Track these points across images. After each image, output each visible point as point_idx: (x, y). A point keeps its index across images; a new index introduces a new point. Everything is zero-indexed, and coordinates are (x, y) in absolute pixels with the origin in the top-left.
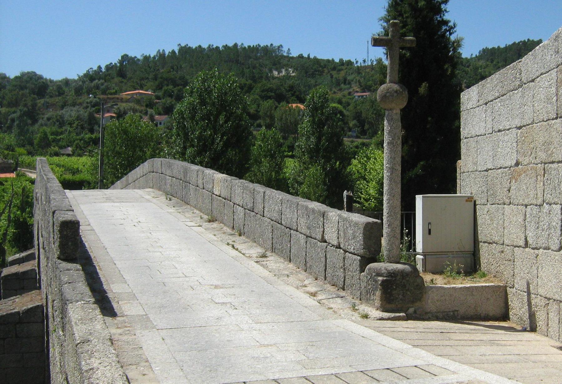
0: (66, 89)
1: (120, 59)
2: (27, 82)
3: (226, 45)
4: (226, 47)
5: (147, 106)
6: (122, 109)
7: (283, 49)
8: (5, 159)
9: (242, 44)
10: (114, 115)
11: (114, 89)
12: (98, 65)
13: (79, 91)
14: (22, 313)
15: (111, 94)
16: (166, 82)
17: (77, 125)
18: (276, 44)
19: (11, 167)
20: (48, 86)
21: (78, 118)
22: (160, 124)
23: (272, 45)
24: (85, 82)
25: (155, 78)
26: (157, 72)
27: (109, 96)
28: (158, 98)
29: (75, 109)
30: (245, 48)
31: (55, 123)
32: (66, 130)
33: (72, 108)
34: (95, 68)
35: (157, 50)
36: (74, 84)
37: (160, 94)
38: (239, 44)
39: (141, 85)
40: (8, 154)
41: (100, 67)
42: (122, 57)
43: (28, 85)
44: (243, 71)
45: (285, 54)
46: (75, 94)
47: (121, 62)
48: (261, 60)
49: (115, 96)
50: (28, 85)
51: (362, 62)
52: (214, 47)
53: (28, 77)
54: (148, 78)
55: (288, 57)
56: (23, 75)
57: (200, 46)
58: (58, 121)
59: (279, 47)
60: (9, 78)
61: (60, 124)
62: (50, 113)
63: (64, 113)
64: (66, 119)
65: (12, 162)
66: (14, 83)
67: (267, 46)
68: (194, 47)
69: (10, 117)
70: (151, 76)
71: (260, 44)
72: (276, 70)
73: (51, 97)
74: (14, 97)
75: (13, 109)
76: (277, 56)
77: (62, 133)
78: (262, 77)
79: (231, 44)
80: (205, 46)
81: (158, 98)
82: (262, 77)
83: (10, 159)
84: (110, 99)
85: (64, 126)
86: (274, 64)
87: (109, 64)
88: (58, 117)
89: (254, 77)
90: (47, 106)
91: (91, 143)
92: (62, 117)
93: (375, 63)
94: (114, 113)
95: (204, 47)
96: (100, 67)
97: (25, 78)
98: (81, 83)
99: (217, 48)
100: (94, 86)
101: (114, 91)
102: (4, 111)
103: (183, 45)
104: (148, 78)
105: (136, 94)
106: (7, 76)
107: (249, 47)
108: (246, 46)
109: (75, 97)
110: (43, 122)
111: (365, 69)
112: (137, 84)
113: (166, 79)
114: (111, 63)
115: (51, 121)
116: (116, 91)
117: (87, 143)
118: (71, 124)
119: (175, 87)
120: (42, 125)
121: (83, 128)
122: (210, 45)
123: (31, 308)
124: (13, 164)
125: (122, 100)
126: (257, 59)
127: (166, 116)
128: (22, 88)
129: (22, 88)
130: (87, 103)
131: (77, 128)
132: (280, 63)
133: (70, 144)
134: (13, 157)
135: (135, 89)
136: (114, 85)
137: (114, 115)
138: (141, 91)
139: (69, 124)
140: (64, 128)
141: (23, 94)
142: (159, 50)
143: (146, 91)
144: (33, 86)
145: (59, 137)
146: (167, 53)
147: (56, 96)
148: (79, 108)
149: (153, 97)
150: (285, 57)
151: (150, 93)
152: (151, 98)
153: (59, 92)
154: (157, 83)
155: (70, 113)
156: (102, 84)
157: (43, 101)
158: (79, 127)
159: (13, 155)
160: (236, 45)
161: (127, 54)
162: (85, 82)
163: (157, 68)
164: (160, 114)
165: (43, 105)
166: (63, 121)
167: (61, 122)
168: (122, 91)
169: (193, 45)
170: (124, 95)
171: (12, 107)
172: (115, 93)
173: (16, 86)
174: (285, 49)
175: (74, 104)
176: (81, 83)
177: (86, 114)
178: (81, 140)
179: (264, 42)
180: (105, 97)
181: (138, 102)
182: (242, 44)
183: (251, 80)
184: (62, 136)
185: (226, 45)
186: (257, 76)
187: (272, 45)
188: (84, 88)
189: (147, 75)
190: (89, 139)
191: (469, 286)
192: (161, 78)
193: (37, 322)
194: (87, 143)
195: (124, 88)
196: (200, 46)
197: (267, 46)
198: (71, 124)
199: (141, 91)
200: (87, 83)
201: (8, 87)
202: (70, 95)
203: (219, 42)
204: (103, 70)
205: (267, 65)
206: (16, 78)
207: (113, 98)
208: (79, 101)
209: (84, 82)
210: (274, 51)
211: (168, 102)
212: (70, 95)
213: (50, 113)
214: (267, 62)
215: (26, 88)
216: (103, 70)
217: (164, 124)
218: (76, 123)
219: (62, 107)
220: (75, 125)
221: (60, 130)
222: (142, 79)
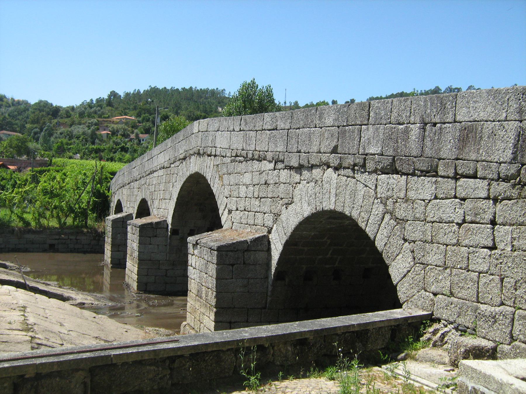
1: (109, 94)
2: (45, 107)
3: (184, 88)
4: (184, 89)
5: (133, 127)
6: (115, 128)
7: (225, 92)
8: (42, 157)
9: (196, 87)
10: (110, 133)
11: (107, 114)
14: (250, 242)
15: (105, 118)
16: (143, 112)
17: (83, 138)
18: (220, 88)
19: (46, 163)
20: (60, 110)
21: (84, 133)
22: (143, 140)
23: (217, 89)
24: (86, 109)
25: (135, 108)
26: (136, 105)
27: (104, 119)
28: (139, 122)
29: (81, 126)
30: (198, 90)
31: (66, 137)
32: (74, 142)
33: (79, 126)
34: (88, 101)
35: (134, 89)
36: (78, 110)
38: (194, 87)
39: (125, 113)
40: (44, 154)
41: (92, 100)
42: (111, 92)
44: (198, 106)
45: (227, 96)
47: (109, 96)
49: (108, 119)
50: (45, 109)
51: (283, 103)
52: (176, 88)
53: (45, 103)
54: (129, 109)
55: (229, 98)
56: (41, 101)
57: (165, 88)
58: (68, 135)
59: (222, 90)
60: (30, 104)
61: (70, 137)
62: (62, 129)
63: (73, 129)
64: (74, 133)
65: (47, 159)
67: (214, 89)
68: (161, 89)
69: (33, 131)
70: (132, 107)
72: (221, 107)
73: (62, 118)
74: (36, 117)
75: (35, 126)
77: (71, 144)
79: (187, 87)
80: (169, 88)
81: (139, 122)
82: (212, 111)
84: (105, 121)
85: (72, 139)
86: (219, 103)
87: (98, 98)
88: (68, 133)
89: (206, 111)
90: (59, 124)
91: (94, 152)
92: (71, 132)
93: (293, 104)
94: (110, 131)
96: (92, 100)
97: (42, 104)
98: (83, 109)
99: (177, 89)
100: (93, 112)
101: (108, 116)
102: (29, 127)
103: (153, 87)
104: (129, 109)
105: (123, 119)
106: (29, 102)
107: (201, 89)
108: (199, 88)
110: (57, 136)
111: (285, 109)
112: (122, 112)
113: (144, 110)
114: (100, 98)
115: (63, 135)
116: (109, 116)
117: (91, 152)
118: (78, 138)
119: (150, 115)
120: (56, 138)
121: (86, 141)
122: (172, 87)
123: (259, 238)
124: (48, 161)
125: (113, 123)
126: (206, 98)
128: (41, 111)
129: (41, 111)
130: (89, 123)
131: (82, 140)
132: (223, 102)
133: (78, 152)
134: (48, 156)
135: (122, 115)
136: (107, 111)
138: (127, 117)
139: (77, 137)
140: (73, 141)
141: (43, 115)
142: (135, 90)
143: (131, 117)
145: (70, 147)
147: (65, 118)
149: (137, 121)
150: (227, 98)
152: (135, 122)
153: (67, 114)
154: (137, 111)
155: (78, 130)
156: (99, 111)
158: (84, 140)
159: (48, 154)
160: (191, 88)
162: (86, 109)
163: (135, 102)
164: (142, 133)
165: (56, 123)
166: (72, 135)
167: (71, 136)
168: (113, 116)
169: (160, 87)
170: (115, 119)
171: (34, 124)
172: (108, 117)
173: (36, 109)
175: (80, 124)
176: (83, 109)
177: (89, 131)
178: (86, 149)
179: (211, 86)
181: (127, 124)
182: (196, 87)
183: (204, 113)
184: (72, 146)
185: (184, 88)
187: (217, 89)
188: (86, 112)
189: (128, 106)
190: (92, 149)
191: (131, 351)
193: (263, 251)
194: (91, 152)
196: (165, 88)
197: (214, 89)
198: (78, 138)
199: (127, 117)
200: (88, 109)
201: (30, 110)
202: (76, 117)
203: (179, 86)
204: (94, 102)
205: (214, 103)
206: (36, 103)
207: (107, 121)
208: (83, 122)
209: (86, 109)
210: (219, 93)
211: (147, 125)
212: (76, 117)
213: (62, 129)
214: (214, 101)
215: (43, 111)
216: (94, 102)
217: (146, 140)
218: (82, 137)
219: (71, 126)
220: (81, 139)
221: (69, 142)
222: (125, 109)
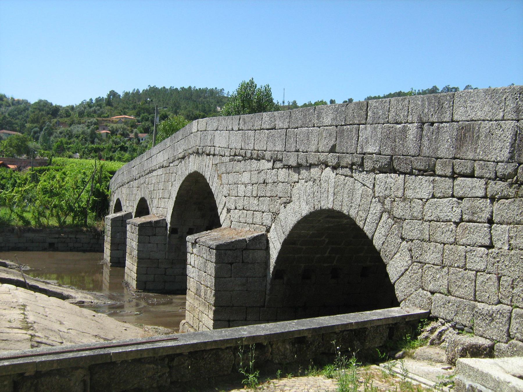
0: (72, 113)
1: (109, 93)
3: (183, 87)
4: (183, 88)
5: (132, 126)
8: (42, 156)
9: (195, 87)
10: (109, 132)
11: (106, 114)
12: (90, 98)
13: (81, 114)
15: (105, 117)
16: (142, 111)
17: (83, 138)
18: (219, 88)
19: (46, 163)
20: (59, 110)
21: (83, 133)
22: (142, 139)
23: (216, 88)
25: (134, 108)
27: (104, 119)
28: (138, 121)
29: (81, 126)
30: (197, 90)
31: (65, 136)
32: (74, 141)
33: (79, 126)
34: (88, 100)
35: (133, 89)
36: (78, 109)
37: (140, 118)
38: (193, 87)
39: (124, 112)
40: (44, 153)
41: (91, 100)
42: (110, 92)
43: (44, 108)
44: (197, 106)
45: (226, 95)
46: (79, 116)
47: (109, 96)
48: (208, 99)
49: (108, 119)
50: (44, 108)
51: (282, 103)
52: (175, 88)
54: (128, 108)
56: (40, 101)
57: (164, 87)
58: (68, 134)
59: (221, 90)
60: (30, 103)
61: (69, 136)
62: (62, 129)
64: (74, 133)
65: (47, 158)
66: (34, 107)
67: (213, 89)
68: (160, 88)
69: (33, 131)
70: (131, 106)
71: (208, 87)
73: (61, 117)
74: (36, 117)
75: (35, 125)
76: (219, 97)
78: (210, 111)
79: (186, 87)
80: (168, 87)
81: (138, 121)
82: (210, 111)
83: (46, 156)
84: (104, 120)
85: (72, 138)
86: (218, 102)
88: (68, 132)
89: (205, 110)
90: (59, 124)
91: (93, 151)
93: (291, 104)
94: (109, 130)
95: (167, 88)
96: (91, 100)
97: (42, 103)
98: (83, 109)
99: (176, 89)
102: (28, 126)
103: (152, 86)
104: (128, 108)
105: (123, 118)
106: (29, 102)
107: (200, 89)
109: (79, 119)
110: (57, 135)
112: (122, 111)
113: (143, 109)
114: (100, 97)
115: (63, 134)
116: (108, 115)
117: (90, 151)
118: (77, 137)
119: (149, 115)
120: (56, 137)
121: (86, 140)
124: (48, 160)
126: (205, 98)
127: (147, 134)
128: (40, 110)
129: (40, 110)
130: (89, 122)
131: (82, 140)
132: (222, 102)
133: (77, 151)
134: (48, 155)
135: (121, 115)
136: (106, 111)
137: (109, 132)
138: (126, 116)
139: (76, 137)
140: (72, 140)
141: (42, 114)
144: (48, 109)
145: (69, 146)
146: (141, 92)
147: (65, 117)
148: (39, 149)
149: (136, 121)
150: (225, 97)
151: (133, 118)
153: (66, 114)
154: (137, 110)
155: (77, 129)
156: (99, 110)
157: (55, 120)
158: (83, 139)
159: (48, 153)
160: (190, 87)
161: (114, 90)
163: (135, 101)
164: (141, 132)
165: (56, 123)
166: (72, 134)
167: (70, 136)
168: (112, 116)
169: (160, 86)
170: (114, 118)
171: (34, 123)
172: (108, 117)
173: (36, 109)
174: (226, 92)
175: (80, 123)
176: (83, 109)
177: (89, 130)
178: (85, 148)
179: (210, 86)
180: (101, 119)
181: (126, 123)
182: (195, 87)
184: (71, 145)
185: (183, 87)
186: (207, 110)
187: (216, 88)
188: (85, 112)
189: (128, 106)
190: (91, 148)
192: (139, 108)
195: (113, 114)
196: (164, 87)
197: (213, 89)
198: (77, 137)
199: (126, 116)
200: (87, 108)
201: (30, 109)
202: (75, 116)
203: (178, 86)
204: (94, 102)
206: (36, 103)
207: (106, 120)
208: (82, 121)
209: (85, 108)
210: (218, 93)
212: (75, 116)
213: (62, 129)
215: (43, 111)
216: (94, 102)
217: (145, 140)
218: (82, 136)
219: (70, 125)
220: (80, 138)
222: (124, 108)
